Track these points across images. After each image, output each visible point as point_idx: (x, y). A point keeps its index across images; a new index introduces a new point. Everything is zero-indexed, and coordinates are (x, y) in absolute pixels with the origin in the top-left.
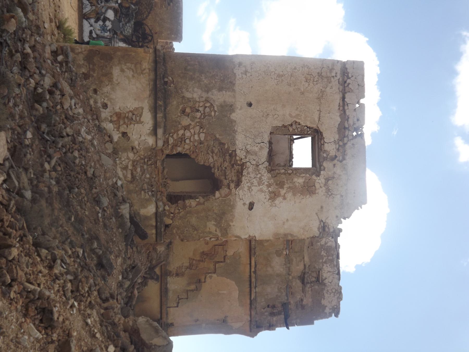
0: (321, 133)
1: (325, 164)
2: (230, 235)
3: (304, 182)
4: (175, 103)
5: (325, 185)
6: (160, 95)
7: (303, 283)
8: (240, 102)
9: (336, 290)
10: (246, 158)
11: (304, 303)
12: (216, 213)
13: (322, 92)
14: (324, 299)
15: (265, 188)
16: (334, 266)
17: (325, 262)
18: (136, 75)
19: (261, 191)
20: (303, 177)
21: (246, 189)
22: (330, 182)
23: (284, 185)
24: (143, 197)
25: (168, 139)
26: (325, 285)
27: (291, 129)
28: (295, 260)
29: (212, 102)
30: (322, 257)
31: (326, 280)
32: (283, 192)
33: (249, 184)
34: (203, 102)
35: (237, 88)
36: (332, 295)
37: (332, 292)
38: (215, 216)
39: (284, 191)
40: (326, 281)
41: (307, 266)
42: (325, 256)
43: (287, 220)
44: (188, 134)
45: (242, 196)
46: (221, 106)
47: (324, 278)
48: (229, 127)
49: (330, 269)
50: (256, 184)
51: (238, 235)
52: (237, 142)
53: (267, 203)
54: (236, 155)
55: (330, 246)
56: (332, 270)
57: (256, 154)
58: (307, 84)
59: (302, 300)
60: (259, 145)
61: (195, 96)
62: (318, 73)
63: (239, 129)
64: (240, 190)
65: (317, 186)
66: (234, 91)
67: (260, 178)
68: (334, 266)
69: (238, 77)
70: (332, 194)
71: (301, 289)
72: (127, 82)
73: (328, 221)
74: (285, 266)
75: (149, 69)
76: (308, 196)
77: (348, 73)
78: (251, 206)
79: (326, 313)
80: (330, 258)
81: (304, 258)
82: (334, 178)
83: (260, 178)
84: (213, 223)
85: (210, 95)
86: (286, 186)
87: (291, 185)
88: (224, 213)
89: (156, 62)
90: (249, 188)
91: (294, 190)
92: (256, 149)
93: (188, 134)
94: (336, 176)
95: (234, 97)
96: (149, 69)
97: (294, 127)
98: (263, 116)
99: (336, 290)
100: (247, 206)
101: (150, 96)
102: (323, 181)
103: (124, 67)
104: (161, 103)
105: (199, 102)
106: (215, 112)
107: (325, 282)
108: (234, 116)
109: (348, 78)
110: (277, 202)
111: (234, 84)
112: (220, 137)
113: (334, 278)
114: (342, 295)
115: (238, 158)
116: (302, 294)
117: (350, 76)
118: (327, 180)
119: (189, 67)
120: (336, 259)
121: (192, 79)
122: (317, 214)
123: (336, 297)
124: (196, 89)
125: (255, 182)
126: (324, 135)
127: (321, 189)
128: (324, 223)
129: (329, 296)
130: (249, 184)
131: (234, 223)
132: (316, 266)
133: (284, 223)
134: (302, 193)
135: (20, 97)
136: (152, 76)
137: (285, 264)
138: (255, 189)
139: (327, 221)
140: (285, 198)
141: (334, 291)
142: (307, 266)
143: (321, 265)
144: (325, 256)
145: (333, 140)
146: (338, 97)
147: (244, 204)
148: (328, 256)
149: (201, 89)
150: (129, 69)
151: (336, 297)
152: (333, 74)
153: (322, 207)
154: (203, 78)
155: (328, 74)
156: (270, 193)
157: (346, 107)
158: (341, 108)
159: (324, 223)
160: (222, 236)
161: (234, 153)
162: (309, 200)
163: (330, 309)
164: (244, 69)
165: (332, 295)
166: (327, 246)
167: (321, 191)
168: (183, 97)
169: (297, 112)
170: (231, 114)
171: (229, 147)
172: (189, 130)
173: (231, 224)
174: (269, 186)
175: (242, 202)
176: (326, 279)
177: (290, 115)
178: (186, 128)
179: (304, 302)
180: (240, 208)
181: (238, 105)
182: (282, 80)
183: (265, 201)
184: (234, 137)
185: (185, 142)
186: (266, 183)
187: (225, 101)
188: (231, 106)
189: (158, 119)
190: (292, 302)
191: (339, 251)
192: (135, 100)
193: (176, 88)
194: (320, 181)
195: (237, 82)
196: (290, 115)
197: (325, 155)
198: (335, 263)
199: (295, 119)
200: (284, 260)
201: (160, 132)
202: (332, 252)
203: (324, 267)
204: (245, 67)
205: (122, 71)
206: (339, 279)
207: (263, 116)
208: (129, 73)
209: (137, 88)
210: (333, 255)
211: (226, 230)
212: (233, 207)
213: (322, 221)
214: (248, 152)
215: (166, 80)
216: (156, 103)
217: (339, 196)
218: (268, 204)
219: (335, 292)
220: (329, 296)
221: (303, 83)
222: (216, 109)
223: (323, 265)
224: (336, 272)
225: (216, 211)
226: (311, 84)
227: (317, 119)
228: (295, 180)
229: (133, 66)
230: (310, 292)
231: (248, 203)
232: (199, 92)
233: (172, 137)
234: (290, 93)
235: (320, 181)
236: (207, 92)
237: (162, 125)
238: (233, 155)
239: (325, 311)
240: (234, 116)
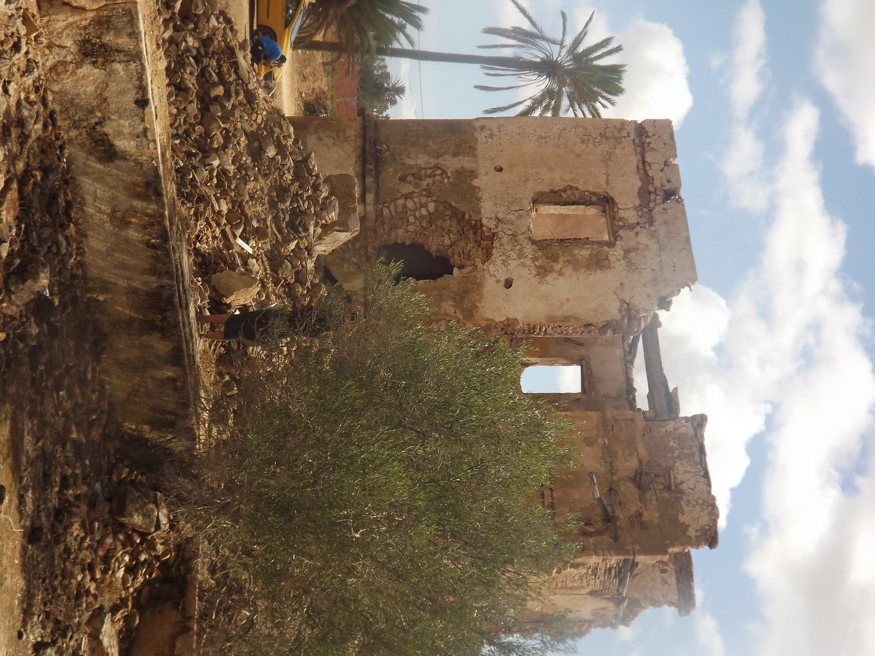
0: (612, 199)
1: (621, 233)
2: (476, 318)
3: (590, 255)
4: (391, 170)
5: (624, 258)
6: (369, 158)
7: (639, 486)
8: (485, 167)
9: (704, 501)
10: (497, 227)
11: (644, 518)
12: (454, 292)
13: (610, 155)
14: (683, 514)
15: (528, 262)
16: (696, 464)
17: (679, 457)
18: (337, 142)
19: (523, 265)
20: (588, 249)
21: (499, 263)
22: (632, 254)
23: (559, 258)
24: (345, 269)
25: (382, 210)
26: (681, 491)
27: (564, 196)
28: (620, 452)
29: (444, 168)
30: (672, 450)
31: (684, 485)
32: (557, 267)
33: (503, 258)
34: (431, 168)
35: (479, 152)
36: (698, 508)
37: (698, 504)
38: (452, 295)
39: (560, 266)
40: (684, 487)
41: (645, 462)
42: (677, 449)
43: (568, 300)
44: (410, 204)
45: (494, 272)
46: (458, 171)
47: (678, 481)
48: (472, 195)
49: (689, 468)
50: (515, 257)
51: (490, 317)
52: (483, 211)
53: (533, 280)
54: (482, 225)
55: (683, 434)
56: (693, 470)
57: (512, 223)
58: (584, 146)
59: (641, 515)
60: (516, 214)
61: (419, 162)
62: (601, 134)
63: (485, 196)
64: (490, 264)
65: (612, 259)
66: (476, 156)
67: (521, 250)
68: (696, 464)
69: (480, 141)
70: (637, 268)
71: (637, 496)
72: (326, 149)
73: (635, 301)
74: (602, 461)
75: (355, 136)
76: (597, 272)
77: (647, 132)
78: (508, 284)
79: (690, 537)
80: (686, 451)
81: (637, 450)
82: (637, 249)
83: (521, 250)
84: (450, 303)
85: (441, 161)
86: (562, 259)
87: (570, 258)
88: (466, 292)
89: (364, 128)
90: (504, 262)
91: (576, 265)
92: (513, 217)
93: (410, 204)
94: (641, 247)
95: (476, 162)
96: (355, 136)
97: (569, 192)
98: (520, 181)
99: (704, 501)
100: (502, 284)
101: (356, 162)
102: (622, 253)
103: (321, 135)
104: (371, 167)
105: (426, 169)
106: (449, 178)
107: (681, 487)
108: (476, 182)
109: (647, 137)
110: (549, 278)
111: (476, 149)
112: (457, 206)
113: (698, 481)
114: (717, 509)
115: (484, 229)
116: (641, 505)
117: (650, 134)
118: (627, 251)
119: (410, 133)
120: (697, 453)
121: (414, 145)
122: (614, 292)
123: (706, 512)
124: (420, 156)
125: (513, 255)
126: (617, 200)
127: (618, 263)
128: (628, 304)
129: (692, 509)
130: (503, 258)
131: (482, 304)
132: (661, 462)
133: (562, 304)
134: (588, 267)
135: (91, 568)
136: (360, 142)
137: (602, 458)
138: (513, 264)
139: (633, 301)
140: (561, 274)
141: (701, 502)
142: (645, 462)
143: (671, 461)
144: (677, 449)
145: (632, 205)
146: (634, 160)
147: (498, 282)
148: (683, 449)
149: (429, 155)
150: (328, 137)
151: (706, 512)
152: (624, 134)
153: (622, 284)
154: (430, 143)
155: (616, 134)
156: (537, 267)
157: (648, 168)
158: (642, 172)
159: (628, 304)
160: (464, 318)
161: (479, 223)
162: (599, 277)
163: (697, 531)
164: (489, 132)
165: (698, 508)
166: (679, 434)
167: (619, 266)
168: (403, 163)
169: (572, 176)
170: (472, 180)
171: (470, 216)
172: (412, 199)
173: (478, 304)
174: (535, 259)
175: (494, 279)
176: (682, 482)
177: (561, 179)
178: (406, 197)
179: (646, 517)
180: (491, 286)
181: (482, 170)
182: (546, 143)
183: (530, 277)
184: (478, 204)
185: (408, 221)
186: (530, 256)
187: (462, 167)
188: (472, 172)
189: (367, 183)
190: (622, 516)
191: (702, 437)
192: (336, 167)
193: (392, 155)
194: (615, 253)
195: (480, 147)
196: (561, 179)
197: (621, 223)
198: (697, 459)
199: (569, 183)
200: (600, 451)
201: (370, 197)
202: (690, 442)
203: (678, 464)
204: (490, 130)
205: (320, 139)
206: (709, 485)
207: (520, 181)
208: (330, 142)
209: (339, 155)
210: (691, 448)
211: (471, 312)
212: (480, 285)
213: (625, 302)
214: (499, 220)
215: (378, 147)
216: (364, 166)
217: (648, 271)
218: (535, 281)
219: (703, 504)
220: (692, 509)
221: (578, 144)
222: (449, 174)
223: (675, 462)
224: (702, 473)
225: (454, 290)
226: (591, 145)
227: (603, 183)
228: (576, 252)
229: (334, 134)
230: (654, 502)
231: (503, 279)
232: (426, 158)
233: (388, 207)
234: (558, 155)
235: (616, 252)
236: (437, 158)
237: (374, 190)
238: (477, 227)
239: (688, 533)
240: (476, 182)
